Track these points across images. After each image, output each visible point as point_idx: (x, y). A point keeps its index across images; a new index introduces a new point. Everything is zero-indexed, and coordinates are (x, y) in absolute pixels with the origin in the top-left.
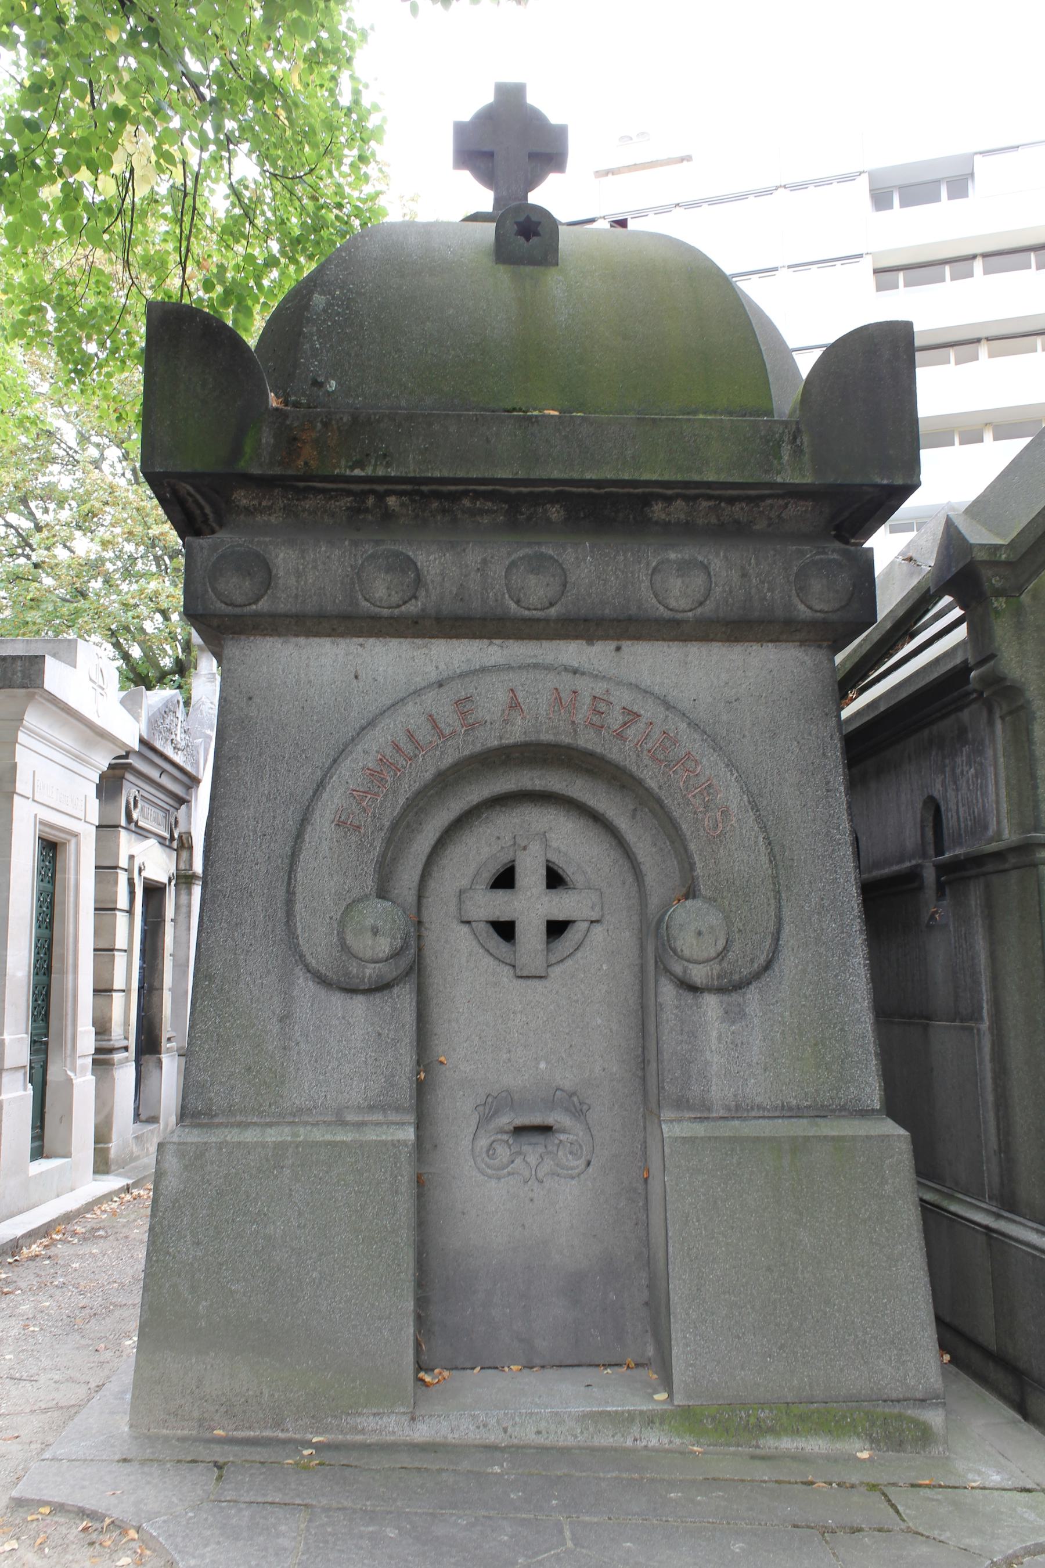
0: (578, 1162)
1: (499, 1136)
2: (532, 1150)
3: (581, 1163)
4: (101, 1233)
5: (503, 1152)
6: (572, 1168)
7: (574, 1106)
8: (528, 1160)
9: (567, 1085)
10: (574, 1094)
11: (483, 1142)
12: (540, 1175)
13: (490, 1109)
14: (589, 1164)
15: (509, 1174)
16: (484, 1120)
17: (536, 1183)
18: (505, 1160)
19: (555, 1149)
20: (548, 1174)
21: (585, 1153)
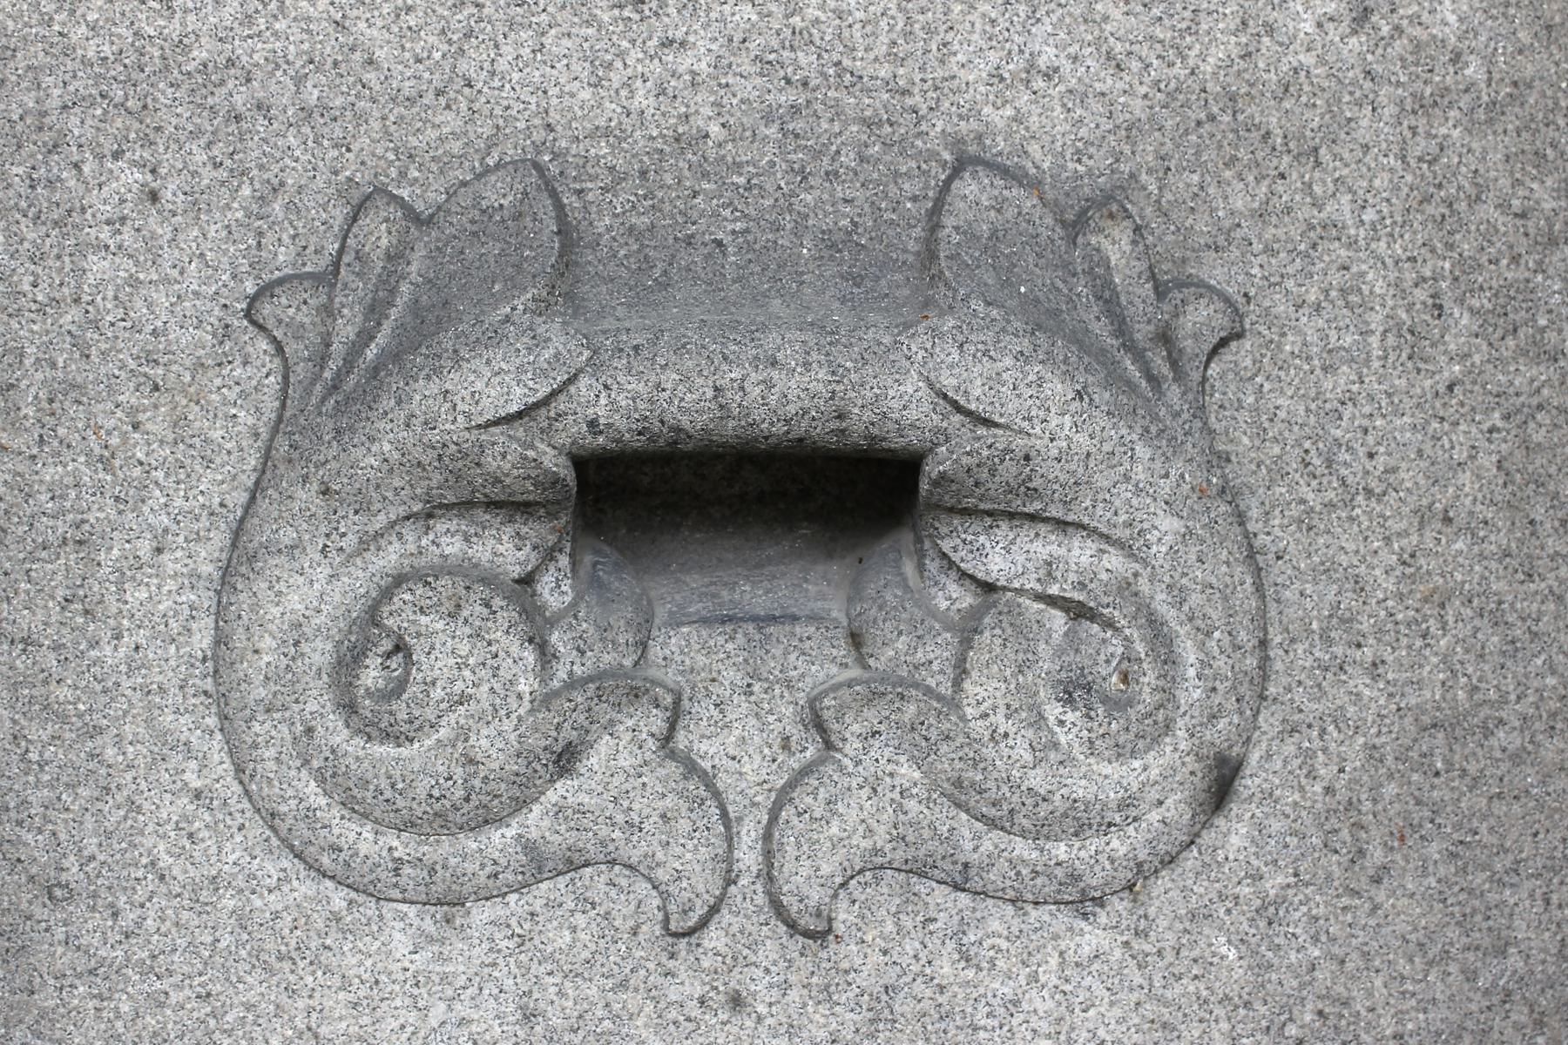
0: (1157, 762)
1: (450, 541)
2: (745, 665)
3: (1162, 773)
4: (372, 675)
5: (481, 681)
6: (1081, 821)
7: (1109, 300)
8: (708, 749)
9: (1046, 130)
10: (1109, 202)
11: (309, 594)
12: (804, 880)
13: (375, 310)
14: (1221, 785)
15: (538, 864)
16: (328, 396)
17: (773, 945)
18: (495, 746)
19: (938, 651)
20: (874, 866)
21: (1191, 693)
